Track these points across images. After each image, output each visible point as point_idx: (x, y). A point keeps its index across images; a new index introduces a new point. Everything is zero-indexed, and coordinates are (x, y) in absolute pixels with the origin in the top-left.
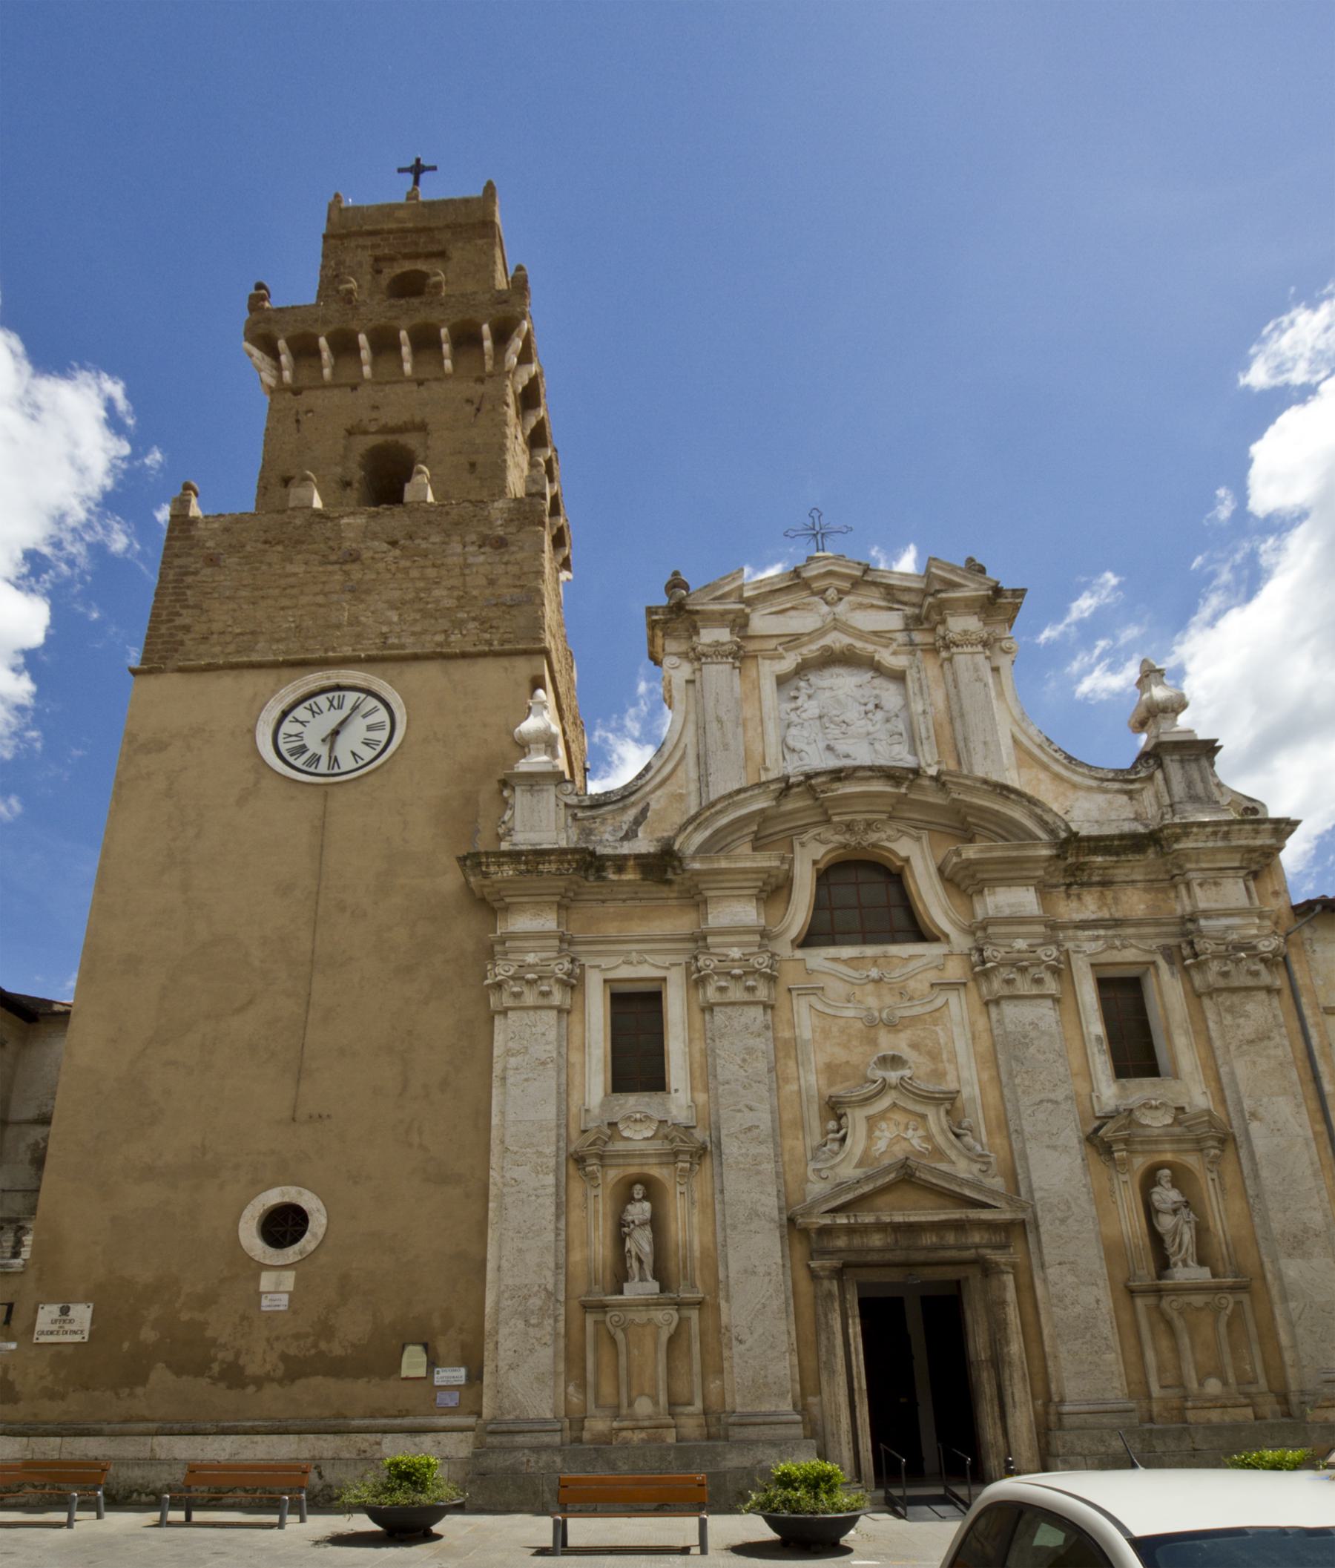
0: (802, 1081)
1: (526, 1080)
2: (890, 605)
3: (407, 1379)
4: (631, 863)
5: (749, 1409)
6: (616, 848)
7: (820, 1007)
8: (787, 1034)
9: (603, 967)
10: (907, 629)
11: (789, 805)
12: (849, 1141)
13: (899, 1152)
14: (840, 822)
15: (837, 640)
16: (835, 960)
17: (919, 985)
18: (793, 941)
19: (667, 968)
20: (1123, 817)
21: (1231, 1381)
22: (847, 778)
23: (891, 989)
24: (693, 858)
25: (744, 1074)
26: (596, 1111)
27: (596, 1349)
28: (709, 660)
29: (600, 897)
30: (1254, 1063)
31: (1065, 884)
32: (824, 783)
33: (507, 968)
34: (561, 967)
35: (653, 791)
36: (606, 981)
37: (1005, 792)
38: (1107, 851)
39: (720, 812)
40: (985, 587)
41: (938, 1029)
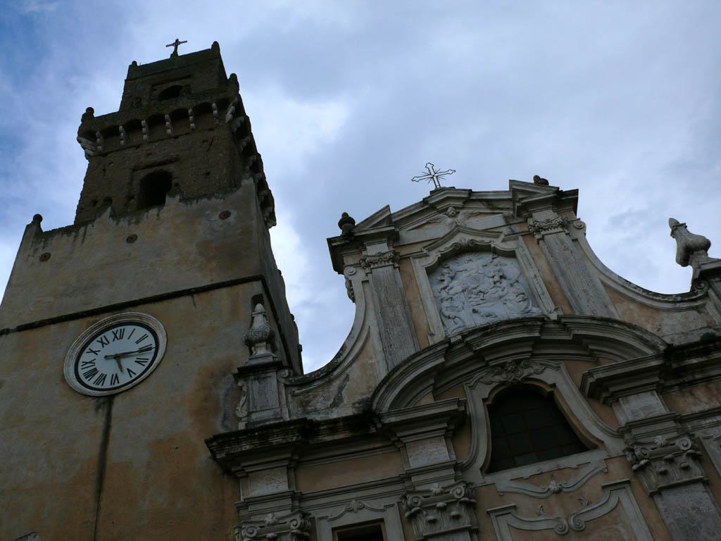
4: (341, 424)
18: (481, 469)
19: (383, 511)
24: (389, 414)
34: (295, 523)
36: (333, 529)
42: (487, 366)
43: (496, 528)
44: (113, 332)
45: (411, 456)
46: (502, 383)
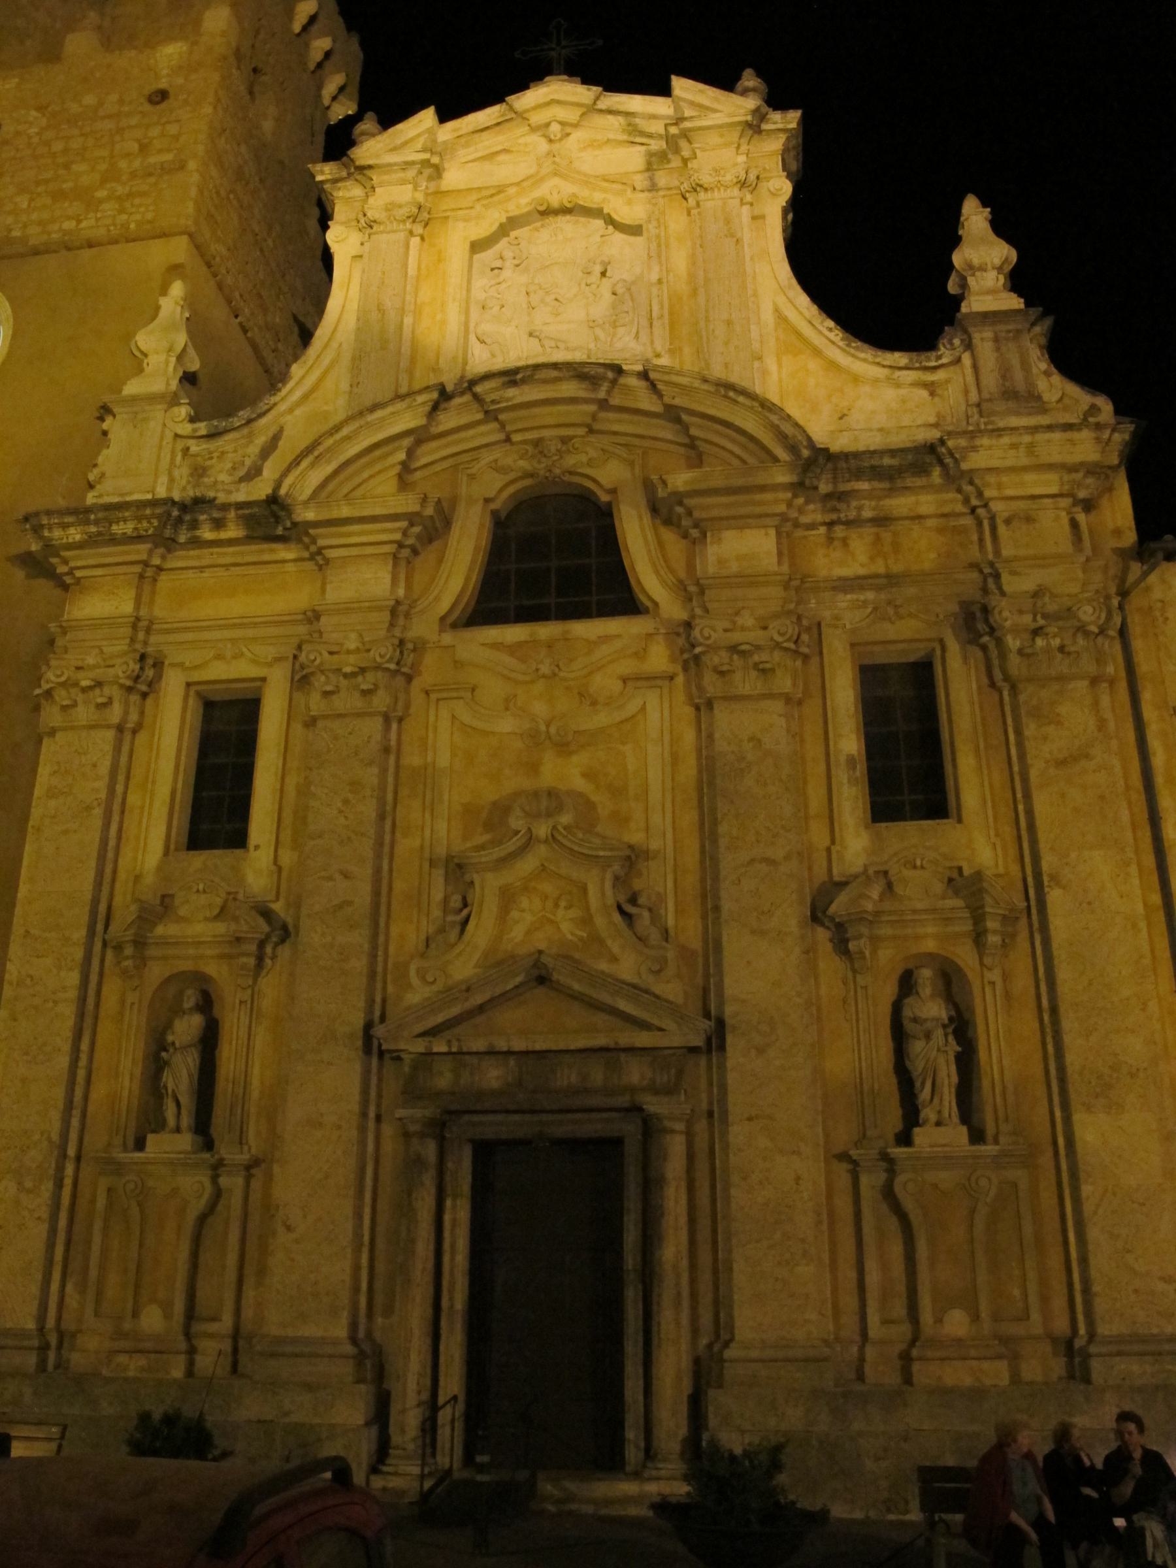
0: (427, 833)
1: (65, 832)
2: (632, 139)
4: (232, 514)
5: (290, 1332)
6: (230, 492)
7: (466, 717)
9: (187, 664)
10: (649, 168)
11: (448, 420)
13: (540, 941)
14: (525, 442)
15: (556, 191)
17: (605, 683)
18: (443, 619)
20: (919, 422)
21: (983, 1315)
22: (524, 381)
23: (568, 688)
25: (342, 820)
26: (149, 879)
27: (106, 1228)
28: (382, 228)
30: (1063, 795)
31: (824, 524)
32: (496, 389)
33: (59, 673)
35: (291, 410)
36: (188, 685)
37: (731, 394)
38: (877, 473)
39: (348, 438)
40: (742, 111)
42: (508, 440)
43: (432, 719)
45: (331, 582)
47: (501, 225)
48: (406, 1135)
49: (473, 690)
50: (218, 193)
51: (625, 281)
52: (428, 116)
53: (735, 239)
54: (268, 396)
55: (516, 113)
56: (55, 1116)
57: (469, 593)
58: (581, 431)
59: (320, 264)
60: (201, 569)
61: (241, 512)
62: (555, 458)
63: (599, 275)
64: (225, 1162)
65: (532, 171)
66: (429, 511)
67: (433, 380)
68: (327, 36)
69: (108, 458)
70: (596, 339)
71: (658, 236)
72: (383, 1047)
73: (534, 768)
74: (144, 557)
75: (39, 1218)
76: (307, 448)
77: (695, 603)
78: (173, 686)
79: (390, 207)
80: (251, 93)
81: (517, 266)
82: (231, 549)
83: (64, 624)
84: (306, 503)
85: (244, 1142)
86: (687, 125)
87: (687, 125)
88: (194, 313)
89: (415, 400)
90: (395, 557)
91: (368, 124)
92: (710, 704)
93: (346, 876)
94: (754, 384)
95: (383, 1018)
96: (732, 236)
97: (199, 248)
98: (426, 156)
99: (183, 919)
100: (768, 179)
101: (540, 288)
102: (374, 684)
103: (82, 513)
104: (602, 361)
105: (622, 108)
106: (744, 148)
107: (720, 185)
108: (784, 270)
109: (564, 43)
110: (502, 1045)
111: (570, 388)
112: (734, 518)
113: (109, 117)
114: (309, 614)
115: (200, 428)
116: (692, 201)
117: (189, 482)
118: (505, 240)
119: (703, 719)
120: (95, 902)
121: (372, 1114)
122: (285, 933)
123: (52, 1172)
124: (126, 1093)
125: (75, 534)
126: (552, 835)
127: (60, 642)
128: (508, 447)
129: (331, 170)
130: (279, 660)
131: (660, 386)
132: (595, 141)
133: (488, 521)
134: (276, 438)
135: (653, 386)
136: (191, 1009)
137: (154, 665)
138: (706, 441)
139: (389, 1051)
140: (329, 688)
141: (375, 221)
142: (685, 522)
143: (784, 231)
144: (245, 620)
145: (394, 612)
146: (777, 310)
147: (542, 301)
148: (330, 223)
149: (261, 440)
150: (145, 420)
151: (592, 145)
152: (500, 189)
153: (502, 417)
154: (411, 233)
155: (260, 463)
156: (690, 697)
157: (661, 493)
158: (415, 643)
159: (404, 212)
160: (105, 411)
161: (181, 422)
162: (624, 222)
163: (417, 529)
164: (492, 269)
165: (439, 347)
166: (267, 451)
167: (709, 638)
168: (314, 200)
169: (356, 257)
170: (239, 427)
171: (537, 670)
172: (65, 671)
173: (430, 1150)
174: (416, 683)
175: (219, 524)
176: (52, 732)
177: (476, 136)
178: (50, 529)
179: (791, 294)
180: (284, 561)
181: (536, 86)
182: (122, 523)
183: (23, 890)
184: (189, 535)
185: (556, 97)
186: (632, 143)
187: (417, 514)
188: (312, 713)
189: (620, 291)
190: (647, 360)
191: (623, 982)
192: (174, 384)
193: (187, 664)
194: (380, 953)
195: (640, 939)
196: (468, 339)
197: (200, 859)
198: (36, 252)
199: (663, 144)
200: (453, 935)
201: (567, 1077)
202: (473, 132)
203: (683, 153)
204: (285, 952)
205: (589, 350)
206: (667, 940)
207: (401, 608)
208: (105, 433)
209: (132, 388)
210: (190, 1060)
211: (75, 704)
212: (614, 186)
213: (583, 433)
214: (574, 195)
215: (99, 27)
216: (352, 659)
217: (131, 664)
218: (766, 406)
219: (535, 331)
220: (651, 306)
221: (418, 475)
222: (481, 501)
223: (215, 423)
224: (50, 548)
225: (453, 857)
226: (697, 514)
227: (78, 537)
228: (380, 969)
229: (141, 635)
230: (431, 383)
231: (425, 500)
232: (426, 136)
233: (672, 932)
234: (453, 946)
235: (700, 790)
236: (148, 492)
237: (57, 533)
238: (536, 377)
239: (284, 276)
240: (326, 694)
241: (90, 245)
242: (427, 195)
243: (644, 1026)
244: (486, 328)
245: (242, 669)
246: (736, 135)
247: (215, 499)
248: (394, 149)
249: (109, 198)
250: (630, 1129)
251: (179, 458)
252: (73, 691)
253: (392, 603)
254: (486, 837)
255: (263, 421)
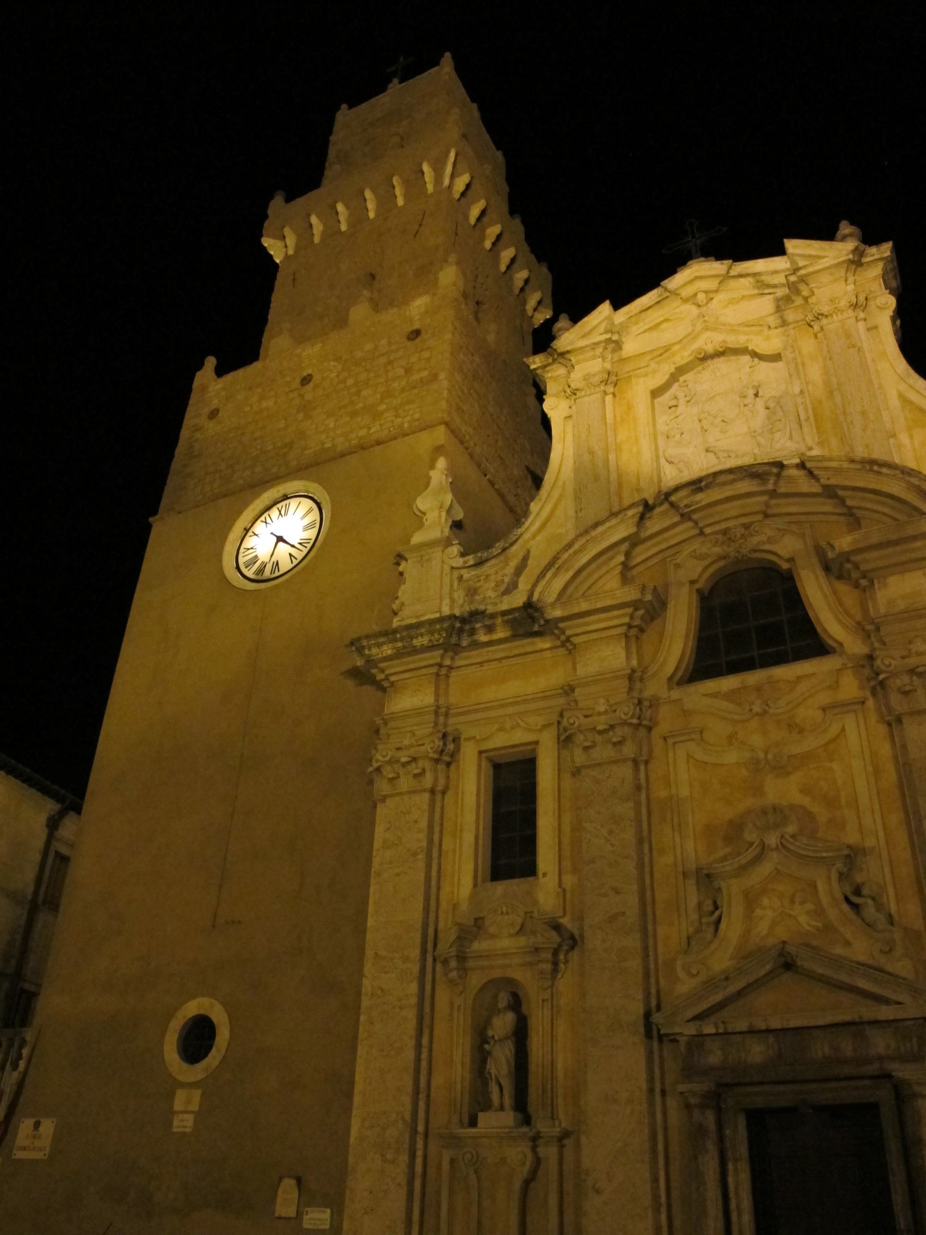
2: (761, 292)
3: (280, 1218)
4: (499, 620)
6: (496, 604)
8: (663, 794)
10: (778, 309)
11: (653, 525)
12: (723, 925)
13: (782, 933)
15: (709, 341)
16: (715, 695)
17: (808, 713)
18: (670, 679)
22: (707, 486)
24: (553, 605)
26: (464, 906)
28: (583, 393)
29: (478, 660)
32: (687, 496)
33: (385, 754)
35: (534, 537)
36: (480, 752)
37: (876, 468)
40: (845, 252)
41: (835, 765)
44: (262, 521)
46: (721, 558)
47: (672, 375)
48: (688, 1107)
49: (701, 732)
50: (462, 391)
51: (775, 397)
52: (605, 308)
53: (857, 349)
54: (515, 530)
55: (669, 292)
56: (407, 1100)
57: (688, 656)
58: (760, 517)
59: (541, 428)
60: (481, 664)
61: (506, 618)
62: (741, 541)
63: (753, 397)
64: (541, 1135)
65: (690, 330)
66: (649, 597)
67: (637, 498)
68: (525, 269)
69: (405, 592)
70: (759, 445)
71: (795, 359)
72: (662, 1032)
73: (758, 790)
74: (438, 660)
75: (399, 1184)
76: (550, 563)
77: (873, 639)
78: (469, 758)
79: (587, 377)
80: (477, 319)
81: (688, 402)
82: (501, 646)
83: (385, 717)
84: (553, 605)
85: (555, 1117)
86: (803, 272)
87: (803, 272)
88: (455, 477)
89: (626, 515)
90: (626, 636)
91: (563, 322)
92: (899, 720)
93: (617, 892)
94: (893, 457)
95: (659, 1008)
96: (854, 346)
97: (453, 432)
98: (608, 336)
99: (493, 937)
100: (875, 298)
101: (709, 415)
102: (623, 737)
103: (389, 634)
104: (766, 461)
105: (750, 271)
106: (851, 279)
107: (838, 310)
108: (901, 364)
109: (697, 235)
110: (762, 1025)
111: (745, 486)
112: (895, 565)
113: (383, 354)
114: (565, 688)
115: (469, 560)
116: (816, 327)
117: (465, 601)
118: (676, 384)
119: (895, 733)
120: (425, 925)
121: (658, 1090)
122: (573, 942)
123: (406, 1146)
124: (459, 1079)
125: (387, 650)
126: (781, 843)
127: (383, 731)
128: (701, 539)
129: (540, 360)
130: (545, 727)
131: (816, 472)
132: (733, 299)
133: (695, 597)
134: (525, 559)
135: (811, 473)
136: (505, 1008)
137: (454, 741)
138: (859, 508)
139: (667, 1035)
140: (587, 744)
141: (577, 390)
142: (855, 575)
143: (895, 334)
144: (518, 699)
145: (630, 678)
146: (901, 396)
147: (712, 424)
148: (544, 397)
149: (513, 563)
150: (429, 560)
151: (733, 302)
152: (667, 348)
153: (694, 517)
154: (605, 393)
155: (516, 579)
156: (882, 719)
157: (830, 555)
158: (650, 701)
159: (596, 380)
160: (400, 558)
161: (455, 557)
162: (765, 353)
163: (640, 612)
164: (670, 408)
165: (638, 472)
166: (519, 571)
167: (890, 665)
168: (531, 381)
169: (566, 418)
170: (497, 555)
171: (751, 710)
172: (389, 752)
173: (710, 1119)
174: (656, 732)
175: (490, 629)
176: (384, 799)
177: (643, 314)
178: (370, 649)
179: (911, 381)
180: (542, 650)
181: (681, 270)
182: (419, 638)
183: (370, 922)
184: (469, 640)
185: (697, 274)
186: (762, 294)
187: (640, 601)
188: (577, 765)
189: (772, 405)
190: (803, 454)
191: (858, 963)
192: (447, 531)
193: (478, 737)
194: (651, 953)
195: (869, 925)
196: (659, 463)
197: (500, 888)
198: (343, 455)
199: (786, 291)
200: (709, 935)
201: (821, 1049)
202: (640, 312)
203: (803, 294)
204: (575, 955)
205: (755, 454)
206: (892, 924)
207: (638, 674)
208: (401, 574)
209: (417, 539)
210: (507, 1051)
211: (397, 777)
212: (753, 328)
213: (761, 519)
214: (724, 341)
215: (371, 299)
216: (603, 718)
217: (436, 741)
218: (907, 472)
219: (709, 447)
220: (798, 412)
221: (635, 572)
222: (687, 585)
223: (479, 555)
224: (371, 663)
225: (702, 869)
226: (863, 567)
227: (389, 652)
228: (652, 966)
229: (442, 719)
230: (636, 500)
231: (643, 588)
232: (605, 322)
233: (896, 917)
234: (710, 942)
235: (903, 795)
236: (436, 612)
237: (374, 651)
238: (717, 482)
239: (515, 441)
240: (586, 749)
241: (379, 443)
242: (613, 363)
243: (887, 1001)
244: (672, 451)
245: (519, 737)
246: (842, 272)
247: (485, 610)
248: (585, 336)
249: (387, 410)
250: (883, 1095)
251: (456, 583)
252: (395, 766)
253: (629, 671)
254: (728, 850)
255: (514, 548)
